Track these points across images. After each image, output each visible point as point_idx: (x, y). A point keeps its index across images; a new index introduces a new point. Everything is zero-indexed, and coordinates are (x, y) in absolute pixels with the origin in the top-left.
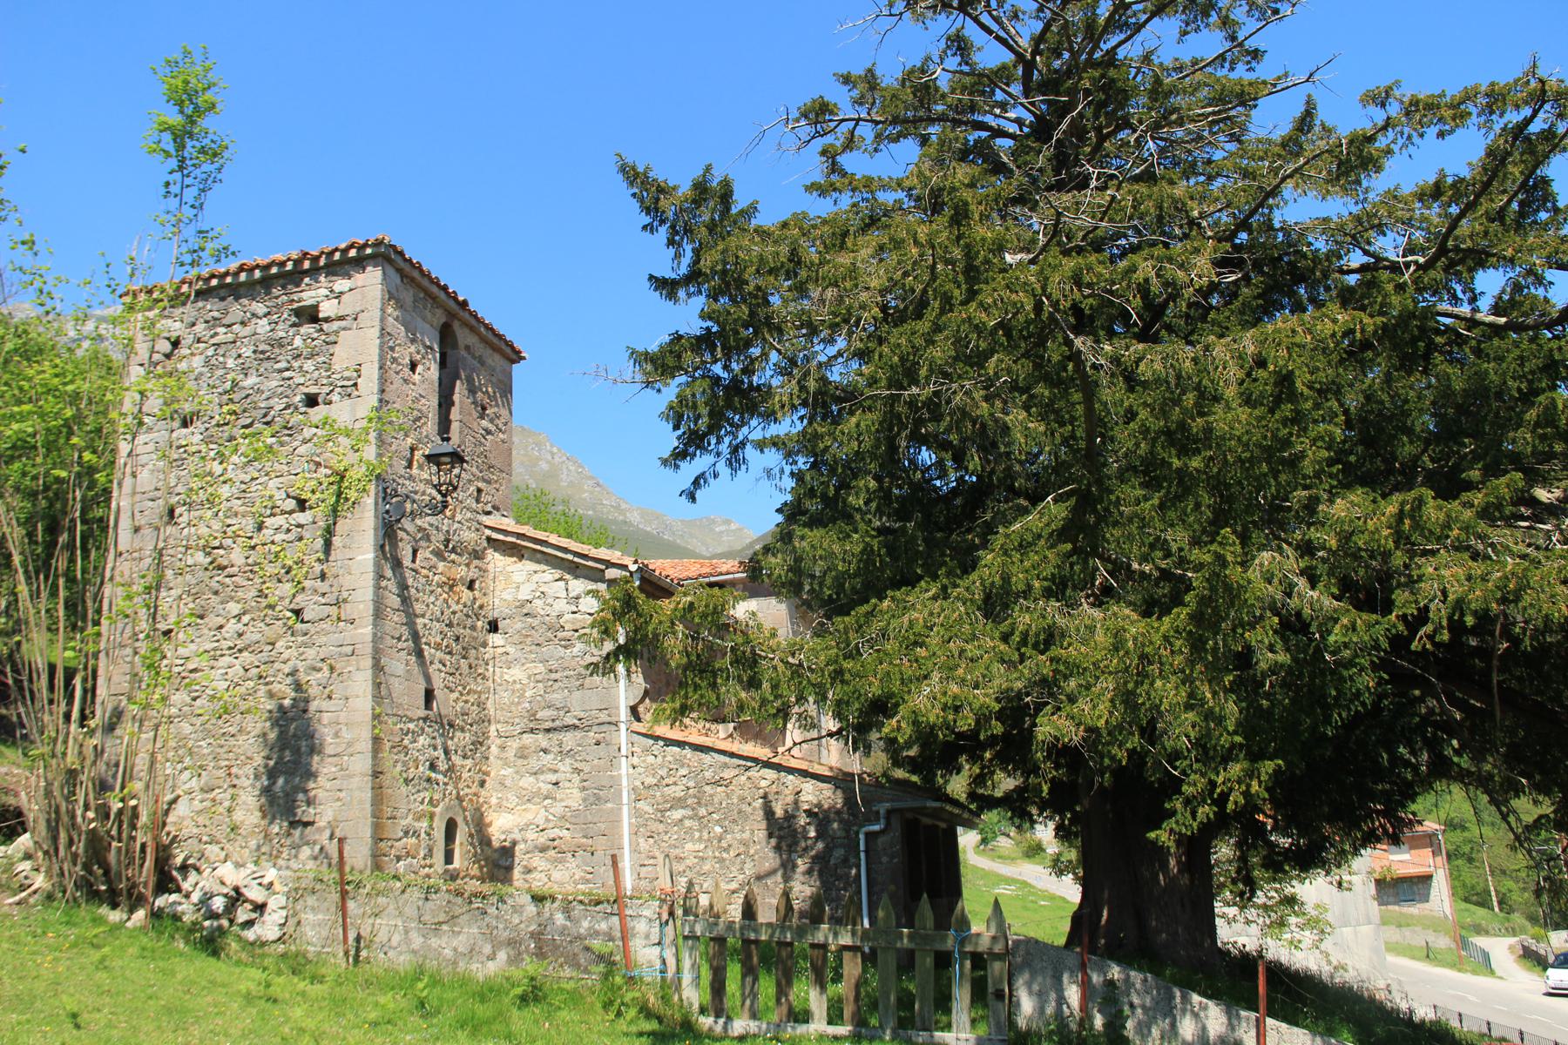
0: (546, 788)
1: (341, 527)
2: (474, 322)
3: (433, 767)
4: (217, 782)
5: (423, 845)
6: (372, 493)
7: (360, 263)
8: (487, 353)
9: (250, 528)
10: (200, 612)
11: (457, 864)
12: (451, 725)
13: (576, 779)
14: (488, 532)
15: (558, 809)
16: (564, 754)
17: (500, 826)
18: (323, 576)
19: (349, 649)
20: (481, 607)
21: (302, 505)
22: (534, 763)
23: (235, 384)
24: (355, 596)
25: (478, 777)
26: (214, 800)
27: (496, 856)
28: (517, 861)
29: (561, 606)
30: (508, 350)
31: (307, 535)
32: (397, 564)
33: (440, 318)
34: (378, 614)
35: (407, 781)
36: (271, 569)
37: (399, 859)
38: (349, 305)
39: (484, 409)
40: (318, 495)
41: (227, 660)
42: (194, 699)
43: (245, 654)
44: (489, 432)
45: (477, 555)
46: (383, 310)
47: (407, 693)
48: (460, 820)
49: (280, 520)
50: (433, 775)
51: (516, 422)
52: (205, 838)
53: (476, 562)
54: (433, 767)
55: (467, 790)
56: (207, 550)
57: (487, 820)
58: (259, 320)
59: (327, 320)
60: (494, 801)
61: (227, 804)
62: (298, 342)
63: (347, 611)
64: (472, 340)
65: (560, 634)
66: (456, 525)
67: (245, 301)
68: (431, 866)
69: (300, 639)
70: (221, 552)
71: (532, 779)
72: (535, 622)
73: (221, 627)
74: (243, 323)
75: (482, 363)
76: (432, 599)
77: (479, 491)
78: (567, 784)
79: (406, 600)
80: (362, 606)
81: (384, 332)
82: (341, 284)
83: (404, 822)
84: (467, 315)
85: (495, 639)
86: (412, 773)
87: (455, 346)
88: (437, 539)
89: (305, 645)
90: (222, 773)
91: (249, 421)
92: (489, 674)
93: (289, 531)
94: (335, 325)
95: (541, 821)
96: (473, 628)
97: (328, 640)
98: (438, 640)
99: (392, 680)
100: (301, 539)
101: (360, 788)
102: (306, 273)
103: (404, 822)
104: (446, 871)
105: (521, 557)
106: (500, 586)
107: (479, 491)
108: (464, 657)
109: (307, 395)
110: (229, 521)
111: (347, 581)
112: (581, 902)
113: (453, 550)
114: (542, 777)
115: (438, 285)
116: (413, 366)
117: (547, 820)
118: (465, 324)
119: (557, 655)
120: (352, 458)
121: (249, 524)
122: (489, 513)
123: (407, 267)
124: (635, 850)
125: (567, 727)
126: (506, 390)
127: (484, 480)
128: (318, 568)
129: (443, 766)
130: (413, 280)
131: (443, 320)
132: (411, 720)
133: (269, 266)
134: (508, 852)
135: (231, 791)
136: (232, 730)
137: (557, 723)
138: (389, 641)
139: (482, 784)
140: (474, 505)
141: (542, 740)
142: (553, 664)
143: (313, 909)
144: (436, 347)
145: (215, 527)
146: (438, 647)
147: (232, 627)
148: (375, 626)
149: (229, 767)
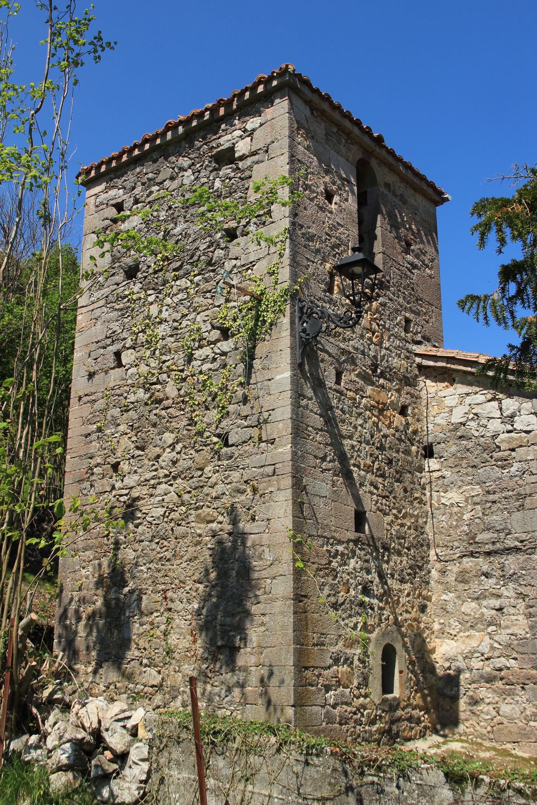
0: (489, 613)
1: (261, 350)
2: (393, 162)
3: (366, 591)
5: (356, 673)
6: (288, 313)
7: (267, 99)
8: (409, 193)
9: (181, 361)
11: (396, 693)
12: (386, 548)
13: (521, 605)
14: (418, 360)
15: (503, 637)
16: (507, 578)
17: (445, 651)
18: (245, 400)
19: (269, 470)
20: (415, 432)
21: (226, 333)
22: (475, 587)
23: (167, 233)
24: (277, 415)
25: (417, 602)
26: (152, 623)
27: (441, 684)
28: (462, 690)
29: (495, 425)
30: (430, 191)
31: (230, 361)
32: (319, 384)
33: (356, 154)
34: (299, 431)
35: (335, 606)
36: (199, 398)
37: (328, 688)
38: (261, 139)
39: (408, 245)
40: (239, 322)
41: (163, 486)
43: (179, 481)
44: (415, 267)
45: (409, 381)
46: (291, 137)
47: (333, 510)
48: (398, 647)
49: (207, 351)
50: (367, 599)
51: (443, 259)
52: (145, 661)
53: (407, 388)
54: (366, 591)
55: (406, 616)
56: (147, 386)
57: (430, 646)
58: (185, 175)
59: (243, 158)
60: (436, 627)
61: (163, 627)
62: (218, 184)
63: (268, 431)
64: (391, 178)
65: (496, 455)
66: (384, 352)
67: (173, 159)
68: (366, 696)
69: (225, 463)
70: (158, 387)
71: (474, 604)
72: (470, 445)
73: (159, 456)
75: (405, 202)
76: (360, 421)
77: (408, 321)
78: (512, 611)
79: (330, 422)
80: (281, 425)
81: (293, 159)
82: (252, 123)
83: (333, 649)
84: (384, 153)
85: (433, 464)
86: (341, 596)
87: (374, 182)
88: (363, 364)
89: (230, 468)
90: (158, 597)
91: (179, 264)
92: (426, 498)
93: (214, 360)
94: (249, 161)
95: (485, 648)
96: (407, 452)
97: (253, 460)
98: (369, 462)
99: (316, 500)
100: (224, 366)
101: (282, 613)
102: (222, 120)
103: (333, 649)
104: (384, 701)
105: (452, 382)
106: (434, 411)
107: (408, 321)
108: (398, 481)
109: (227, 230)
110: (164, 358)
111: (267, 402)
112: (519, 792)
113: (382, 375)
114: (485, 603)
115: (351, 119)
116: (329, 196)
117: (492, 648)
118: (383, 162)
119: (494, 476)
120: (269, 281)
121: (180, 358)
122: (419, 343)
123: (315, 99)
126: (431, 229)
127: (412, 311)
128: (240, 392)
129: (377, 590)
130: (323, 113)
131: (359, 156)
132: (340, 542)
133: (188, 121)
134: (452, 681)
135: (166, 614)
136: (168, 555)
137: (498, 546)
138: (312, 461)
139: (423, 609)
140: (403, 334)
141: (483, 563)
142: (491, 485)
143: (178, 763)
144: (353, 180)
145: (153, 365)
146: (368, 469)
147: (167, 456)
148: (294, 443)
149: (165, 591)
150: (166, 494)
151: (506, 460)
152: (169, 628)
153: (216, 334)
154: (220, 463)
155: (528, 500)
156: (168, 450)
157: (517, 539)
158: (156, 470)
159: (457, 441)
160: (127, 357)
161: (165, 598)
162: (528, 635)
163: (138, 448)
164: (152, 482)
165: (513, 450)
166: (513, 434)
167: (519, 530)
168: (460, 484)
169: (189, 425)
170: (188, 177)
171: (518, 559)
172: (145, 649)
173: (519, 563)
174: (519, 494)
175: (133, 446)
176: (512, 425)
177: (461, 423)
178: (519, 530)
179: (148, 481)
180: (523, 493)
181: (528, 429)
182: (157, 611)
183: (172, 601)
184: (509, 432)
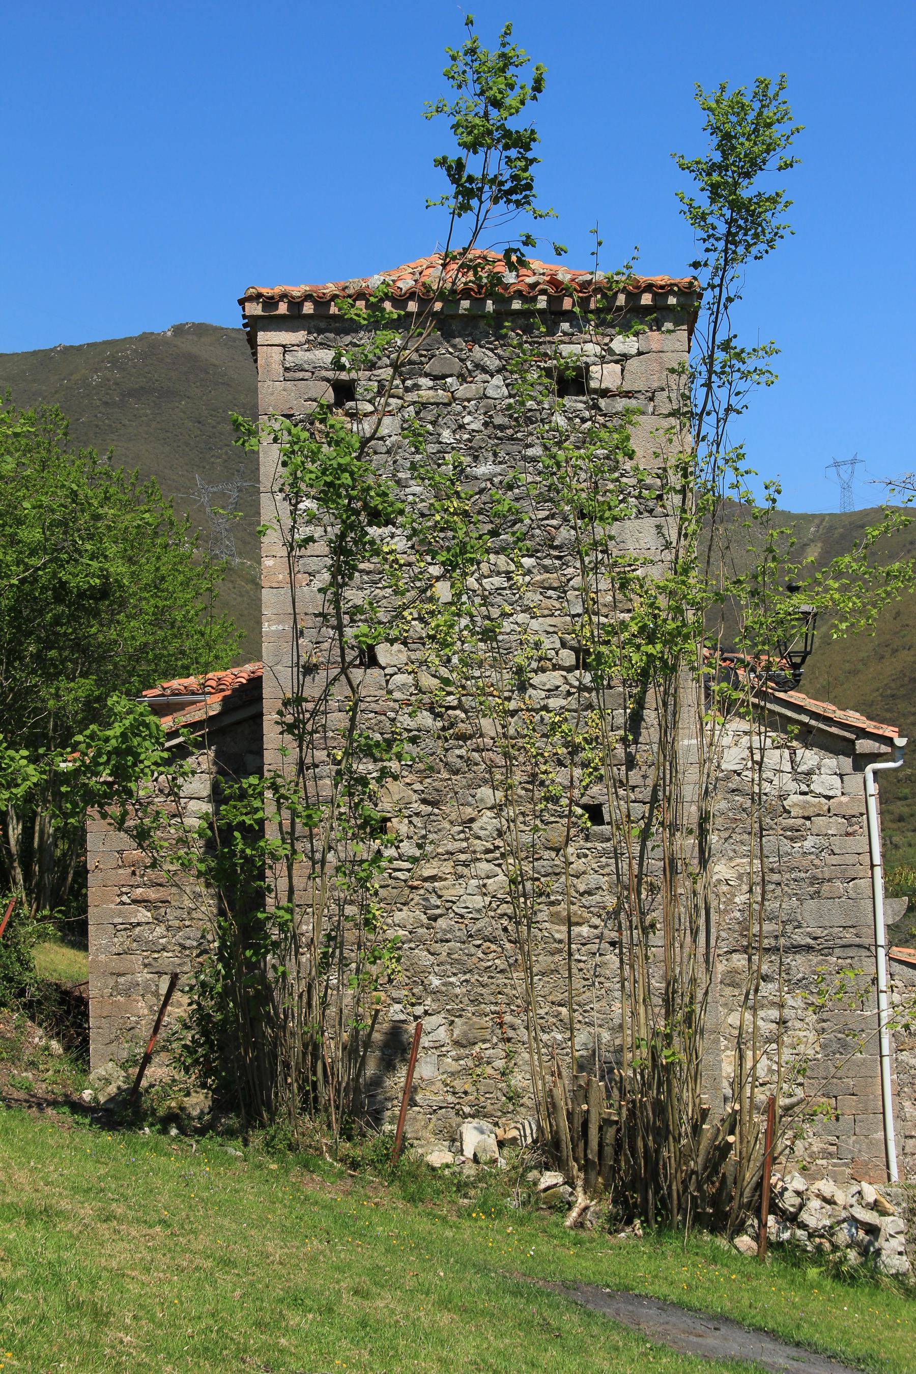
4: (479, 1034)
10: (435, 796)
41: (484, 867)
42: (434, 918)
49: (554, 678)
59: (604, 393)
61: (500, 1064)
73: (472, 820)
74: (462, 378)
78: (798, 1025)
90: (486, 1021)
94: (621, 404)
124: (900, 1117)
125: (797, 949)
147: (487, 822)
150: (488, 877)
151: (797, 831)
152: (511, 1065)
153: (568, 657)
154: (589, 845)
155: (826, 887)
156: (489, 813)
157: (809, 935)
158: (467, 839)
159: (729, 796)
160: (384, 653)
161: (501, 1025)
162: (819, 1056)
163: (424, 801)
164: (463, 857)
165: (808, 818)
166: (808, 797)
167: (812, 923)
168: (732, 854)
169: (528, 783)
170: (496, 387)
171: (810, 960)
172: (466, 1093)
173: (810, 966)
174: (815, 878)
175: (415, 797)
176: (808, 786)
177: (735, 771)
178: (812, 923)
179: (452, 854)
180: (820, 876)
181: (830, 793)
182: (484, 1041)
183: (513, 1027)
184: (805, 793)
